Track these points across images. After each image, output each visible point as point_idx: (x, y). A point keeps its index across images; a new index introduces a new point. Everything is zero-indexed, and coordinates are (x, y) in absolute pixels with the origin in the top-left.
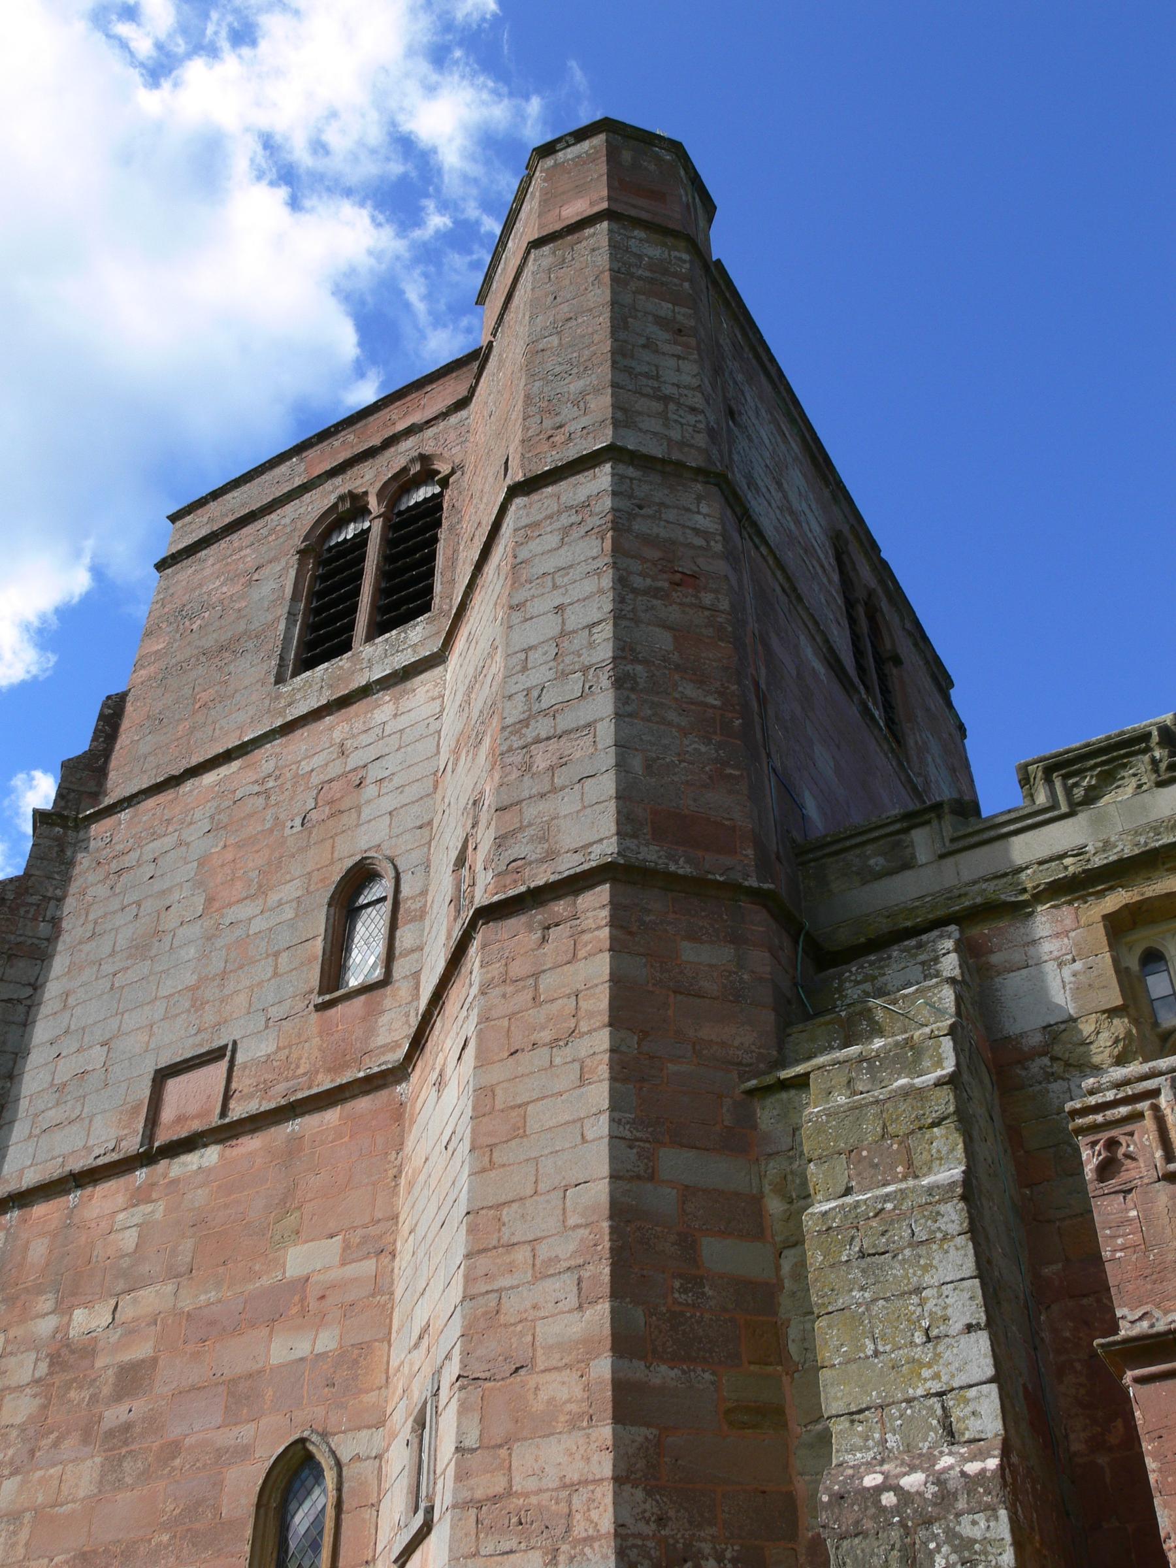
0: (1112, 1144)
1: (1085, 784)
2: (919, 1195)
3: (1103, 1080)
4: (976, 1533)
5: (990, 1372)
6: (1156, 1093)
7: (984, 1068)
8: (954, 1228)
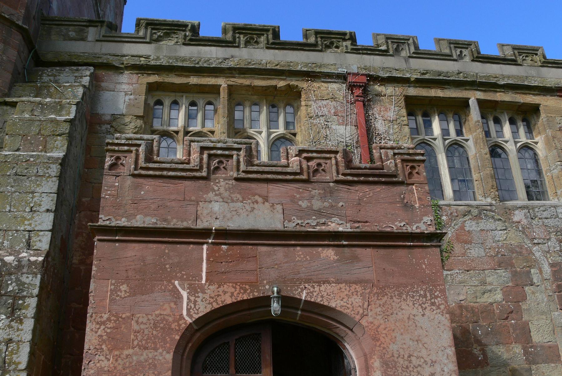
0: (118, 158)
1: (158, 34)
2: (45, 159)
3: (123, 136)
4: (27, 281)
5: (50, 227)
6: (139, 145)
7: (85, 122)
8: (53, 174)
